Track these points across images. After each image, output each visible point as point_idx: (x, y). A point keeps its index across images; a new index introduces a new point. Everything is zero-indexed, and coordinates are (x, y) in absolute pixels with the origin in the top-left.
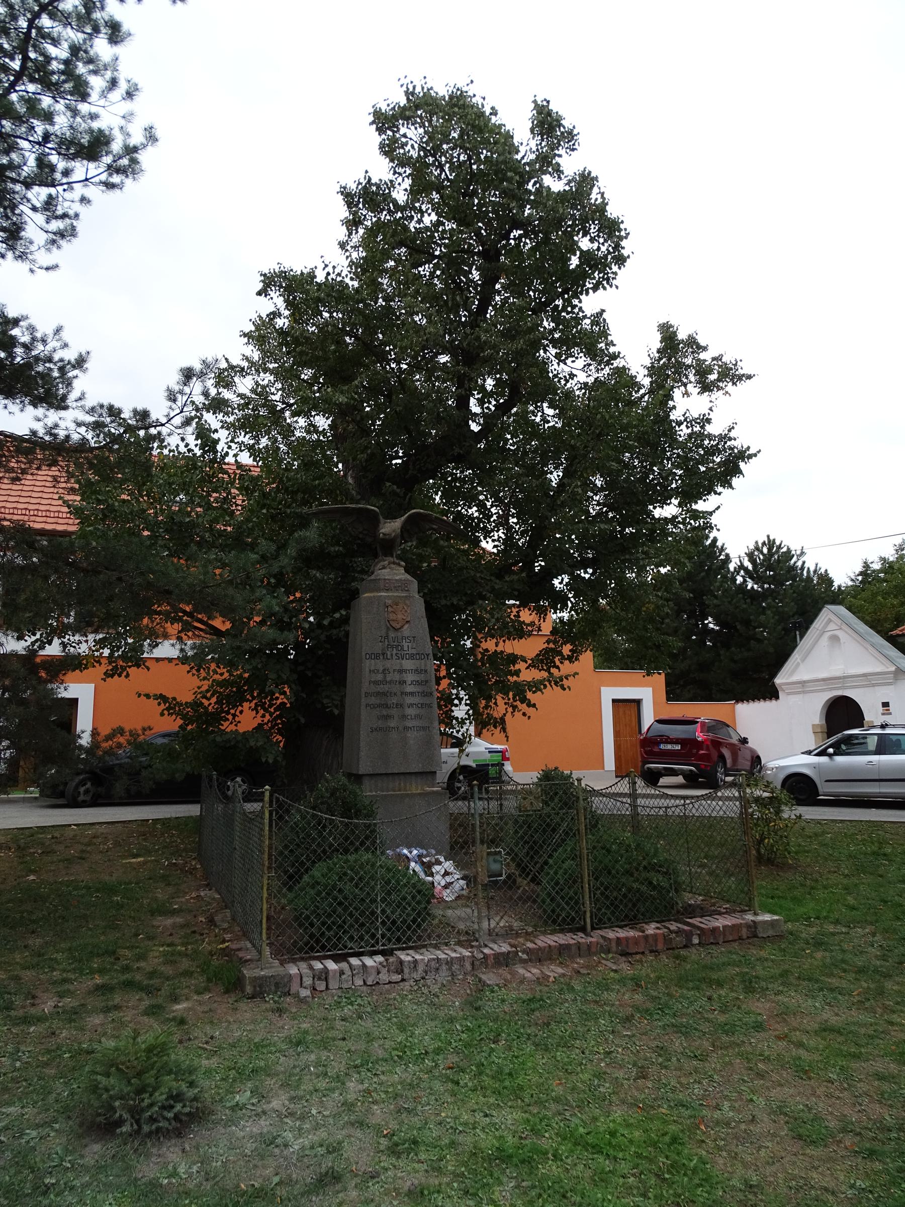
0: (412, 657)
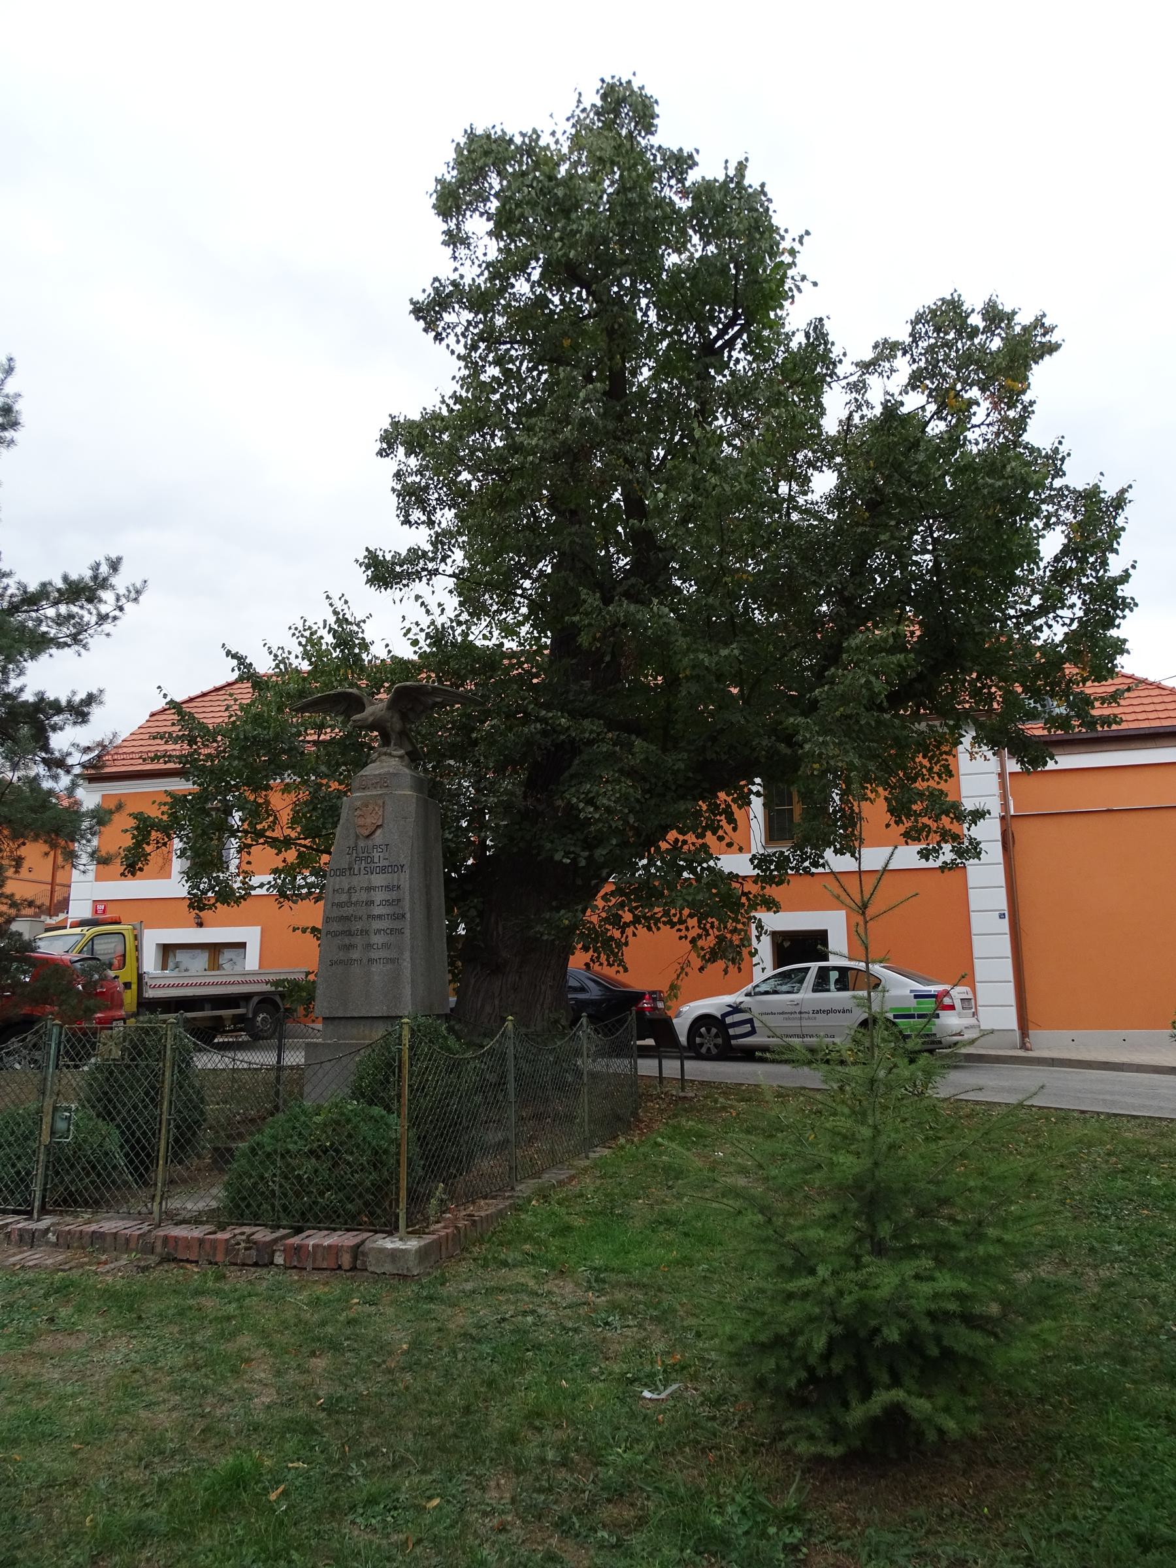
0: (383, 870)
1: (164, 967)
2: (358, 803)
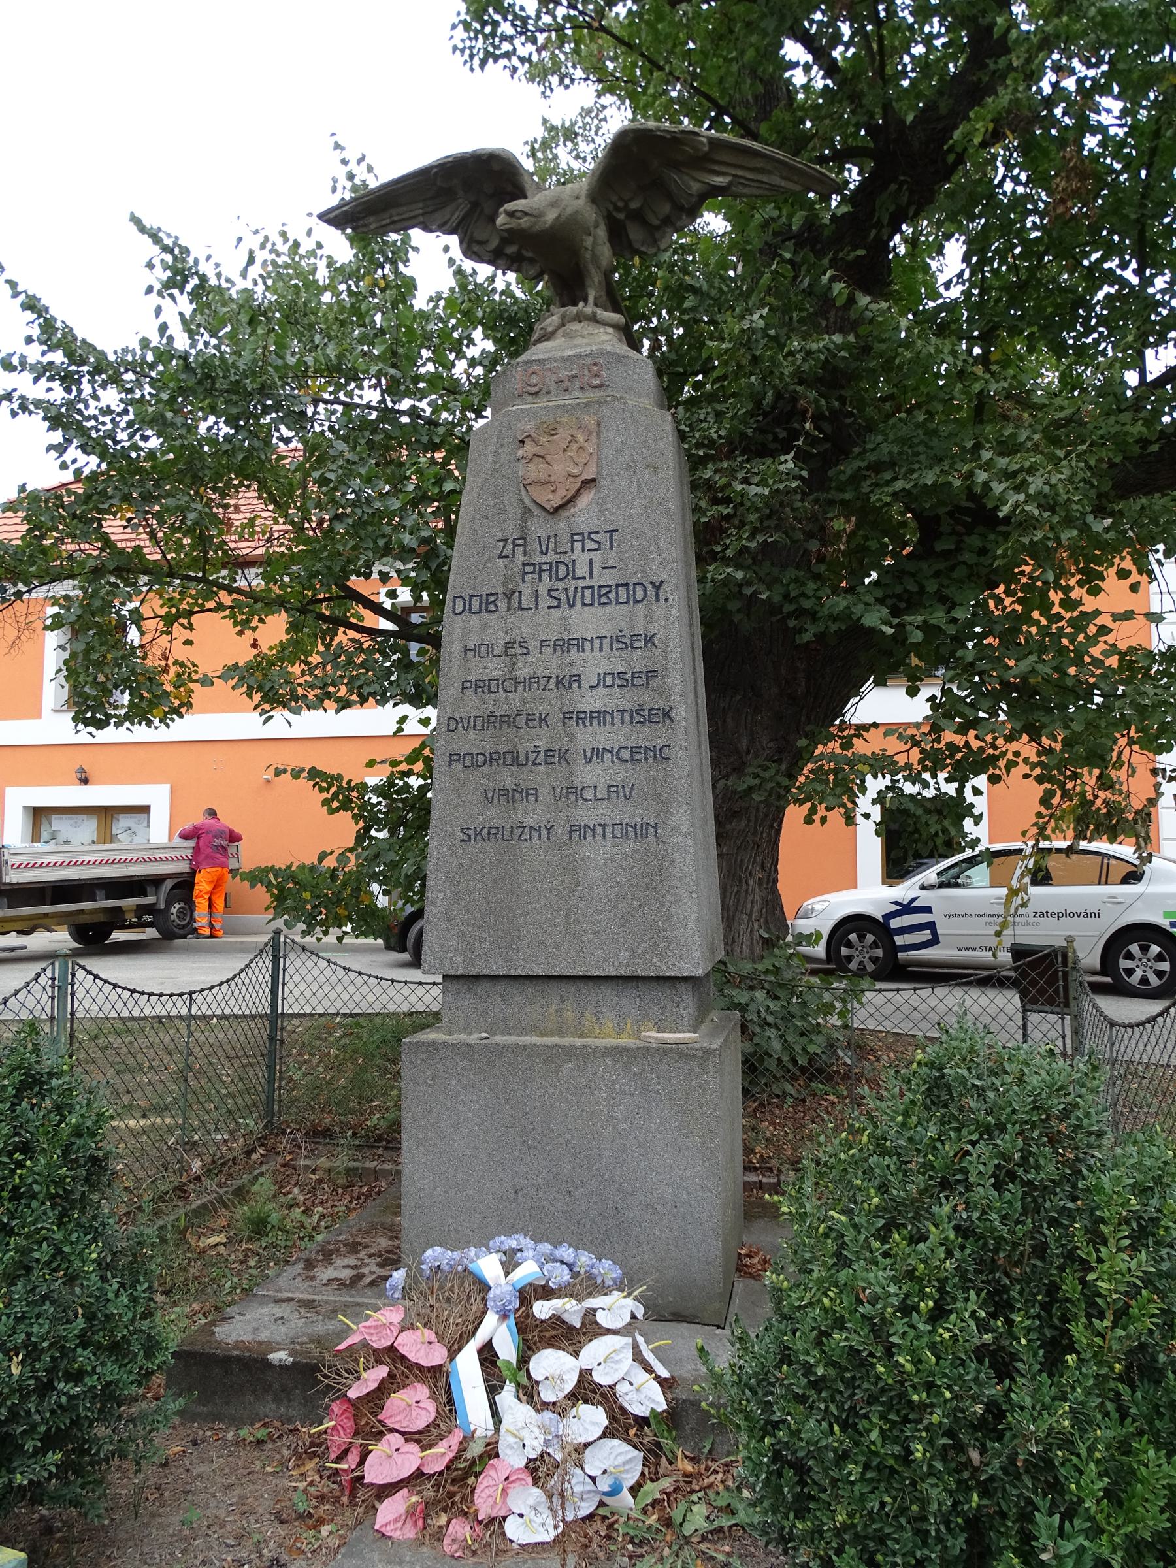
0: (603, 596)
1: (35, 838)
2: (528, 427)
